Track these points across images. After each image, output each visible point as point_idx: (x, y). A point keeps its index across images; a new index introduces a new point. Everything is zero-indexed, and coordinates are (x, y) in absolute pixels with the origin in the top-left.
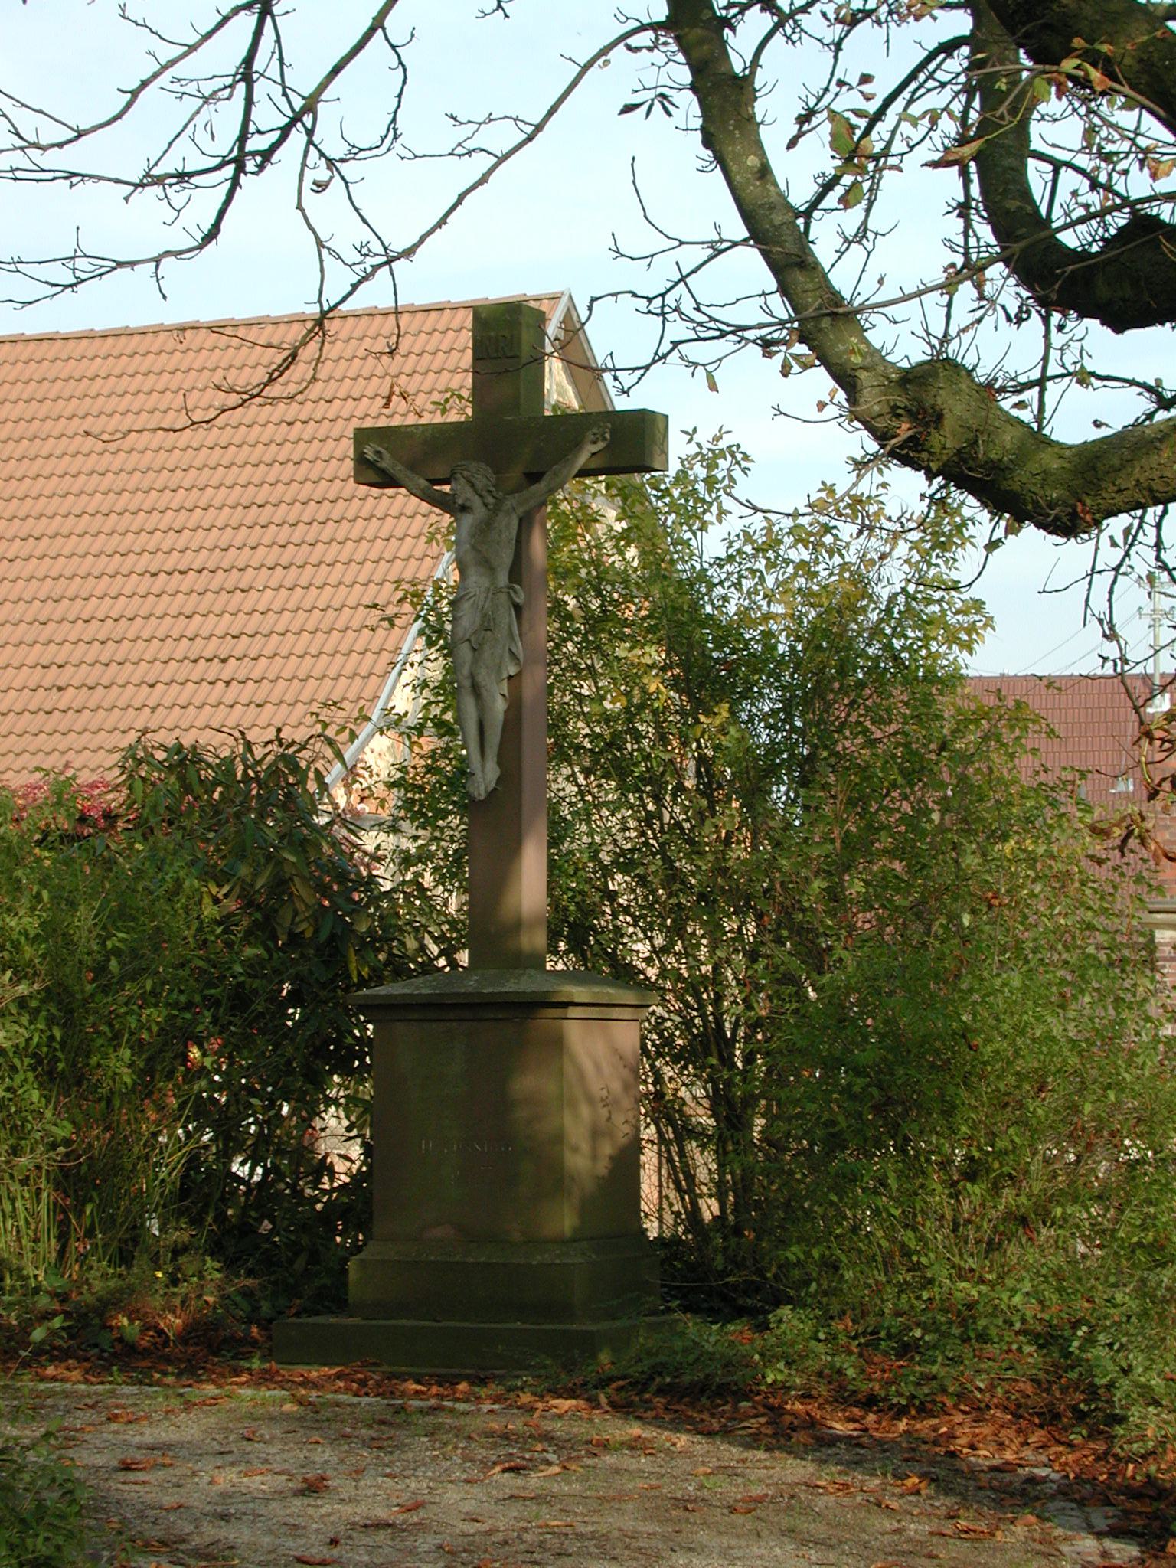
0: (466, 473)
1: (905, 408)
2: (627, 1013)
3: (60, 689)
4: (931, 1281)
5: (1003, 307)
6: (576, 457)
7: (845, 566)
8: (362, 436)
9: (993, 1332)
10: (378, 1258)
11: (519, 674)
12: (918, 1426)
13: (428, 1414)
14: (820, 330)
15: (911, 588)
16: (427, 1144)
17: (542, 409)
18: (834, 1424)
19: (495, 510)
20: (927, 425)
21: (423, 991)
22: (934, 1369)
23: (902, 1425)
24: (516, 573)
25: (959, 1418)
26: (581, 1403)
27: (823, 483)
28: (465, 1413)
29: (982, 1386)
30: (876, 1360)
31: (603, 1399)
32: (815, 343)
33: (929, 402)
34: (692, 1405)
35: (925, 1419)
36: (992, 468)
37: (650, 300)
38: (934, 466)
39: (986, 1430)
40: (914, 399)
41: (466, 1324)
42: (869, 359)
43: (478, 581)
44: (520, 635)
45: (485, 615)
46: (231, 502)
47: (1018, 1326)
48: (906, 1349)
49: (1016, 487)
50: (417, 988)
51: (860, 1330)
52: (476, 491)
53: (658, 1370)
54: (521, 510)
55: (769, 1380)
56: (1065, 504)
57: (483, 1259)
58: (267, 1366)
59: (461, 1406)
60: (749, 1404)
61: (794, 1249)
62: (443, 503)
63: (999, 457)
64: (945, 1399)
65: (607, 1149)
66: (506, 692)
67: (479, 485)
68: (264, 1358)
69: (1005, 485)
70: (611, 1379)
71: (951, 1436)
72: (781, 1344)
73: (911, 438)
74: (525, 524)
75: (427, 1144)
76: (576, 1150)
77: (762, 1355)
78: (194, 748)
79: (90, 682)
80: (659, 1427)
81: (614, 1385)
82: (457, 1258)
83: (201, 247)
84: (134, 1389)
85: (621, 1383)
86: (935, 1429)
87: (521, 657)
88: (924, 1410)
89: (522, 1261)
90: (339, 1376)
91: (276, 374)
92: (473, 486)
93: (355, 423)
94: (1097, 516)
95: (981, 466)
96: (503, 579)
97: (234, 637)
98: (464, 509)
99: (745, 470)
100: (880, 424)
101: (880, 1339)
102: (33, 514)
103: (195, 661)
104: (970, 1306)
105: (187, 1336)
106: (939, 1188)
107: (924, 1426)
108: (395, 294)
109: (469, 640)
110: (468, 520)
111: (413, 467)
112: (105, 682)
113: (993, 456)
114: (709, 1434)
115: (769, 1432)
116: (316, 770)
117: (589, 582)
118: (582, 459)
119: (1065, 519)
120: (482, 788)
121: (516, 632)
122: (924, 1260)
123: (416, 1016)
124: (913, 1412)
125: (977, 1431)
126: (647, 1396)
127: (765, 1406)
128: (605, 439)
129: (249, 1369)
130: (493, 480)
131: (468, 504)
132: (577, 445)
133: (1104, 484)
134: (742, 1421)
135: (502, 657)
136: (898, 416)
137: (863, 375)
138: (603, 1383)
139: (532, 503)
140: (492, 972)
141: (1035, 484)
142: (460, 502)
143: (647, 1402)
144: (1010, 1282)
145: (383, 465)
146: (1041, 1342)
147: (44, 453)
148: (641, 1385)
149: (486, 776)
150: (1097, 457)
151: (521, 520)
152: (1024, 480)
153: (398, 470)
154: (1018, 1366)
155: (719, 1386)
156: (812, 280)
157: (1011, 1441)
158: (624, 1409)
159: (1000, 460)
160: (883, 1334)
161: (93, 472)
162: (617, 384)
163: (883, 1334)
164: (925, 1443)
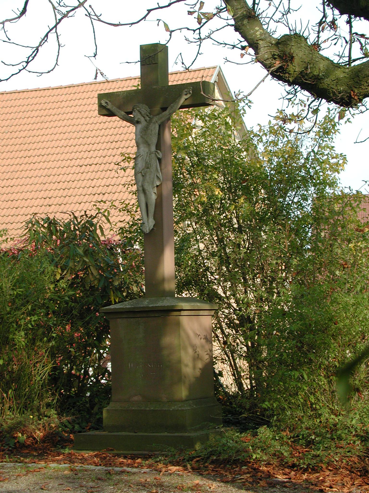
0: (138, 108)
1: (278, 55)
2: (206, 313)
3: (50, 206)
4: (320, 415)
5: (344, 38)
6: (179, 101)
7: (289, 141)
8: (101, 97)
9: (343, 435)
10: (114, 409)
11: (161, 184)
12: (311, 477)
13: (119, 474)
14: (243, 25)
15: (316, 150)
16: (131, 365)
17: (168, 82)
18: (278, 476)
19: (149, 122)
20: (287, 62)
21: (127, 307)
22: (318, 453)
23: (305, 477)
24: (158, 146)
25: (328, 473)
26: (181, 468)
27: (278, 110)
28: (134, 474)
29: (337, 459)
30: (297, 448)
31: (189, 466)
32: (241, 31)
33: (287, 50)
34: (224, 468)
35: (314, 473)
36: (315, 79)
37: (194, 31)
38: (291, 80)
39: (338, 478)
40: (282, 51)
41: (146, 434)
42: (263, 36)
43: (144, 149)
44: (161, 170)
45: (146, 163)
46: (106, 141)
47: (354, 433)
48: (310, 443)
49: (326, 87)
50: (126, 305)
51: (292, 436)
52: (142, 115)
53: (212, 454)
54: (159, 122)
55: (254, 457)
56: (346, 92)
57: (152, 408)
58: (70, 452)
59: (135, 470)
60: (246, 467)
61: (266, 403)
62: (131, 121)
63: (318, 74)
64: (322, 465)
65: (200, 365)
66: (156, 192)
67: (143, 113)
68: (69, 449)
69: (321, 86)
70: (194, 458)
71: (323, 481)
72: (260, 442)
73: (280, 68)
74: (162, 127)
75: (131, 365)
76: (187, 366)
77: (252, 446)
78: (54, 219)
79: (60, 203)
80: (208, 479)
81: (195, 460)
82: (143, 408)
83: (19, 17)
84: (12, 464)
85: (198, 459)
86: (318, 478)
87: (161, 179)
88: (315, 470)
89: (167, 409)
90: (96, 456)
91: (31, 58)
92: (141, 113)
93: (99, 92)
94: (360, 97)
95: (310, 78)
96: (153, 148)
97: (107, 186)
98: (138, 122)
99: (249, 107)
100: (268, 62)
101: (300, 439)
102: (41, 147)
103: (94, 195)
104: (335, 425)
105: (44, 440)
106: (323, 379)
107: (313, 477)
108: (94, 32)
109: (141, 172)
110: (140, 126)
111: (120, 108)
112: (64, 203)
113: (315, 73)
114: (226, 482)
115: (251, 480)
116: (100, 225)
117: (193, 151)
118: (182, 101)
119: (346, 99)
120: (148, 229)
121: (159, 169)
122: (318, 407)
123: (153, 315)
124: (310, 470)
125: (334, 478)
126: (207, 464)
127: (252, 468)
128: (190, 93)
129: (63, 453)
130: (149, 111)
131: (139, 120)
132: (180, 96)
133: (362, 83)
134: (241, 475)
135: (154, 179)
136: (275, 59)
137: (261, 42)
138: (191, 459)
139: (163, 119)
140: (153, 298)
141: (333, 85)
142: (136, 119)
143: (206, 467)
144: (351, 415)
145: (108, 107)
146: (363, 439)
147: (45, 127)
148: (205, 459)
149: (150, 224)
150: (359, 71)
151: (160, 126)
152: (329, 83)
153: (114, 109)
154: (353, 451)
155: (234, 460)
156: (240, 4)
157: (347, 483)
158: (197, 471)
159: (318, 75)
160: (301, 437)
161: (61, 133)
162: (183, 66)
163: (301, 437)
164: (313, 485)
